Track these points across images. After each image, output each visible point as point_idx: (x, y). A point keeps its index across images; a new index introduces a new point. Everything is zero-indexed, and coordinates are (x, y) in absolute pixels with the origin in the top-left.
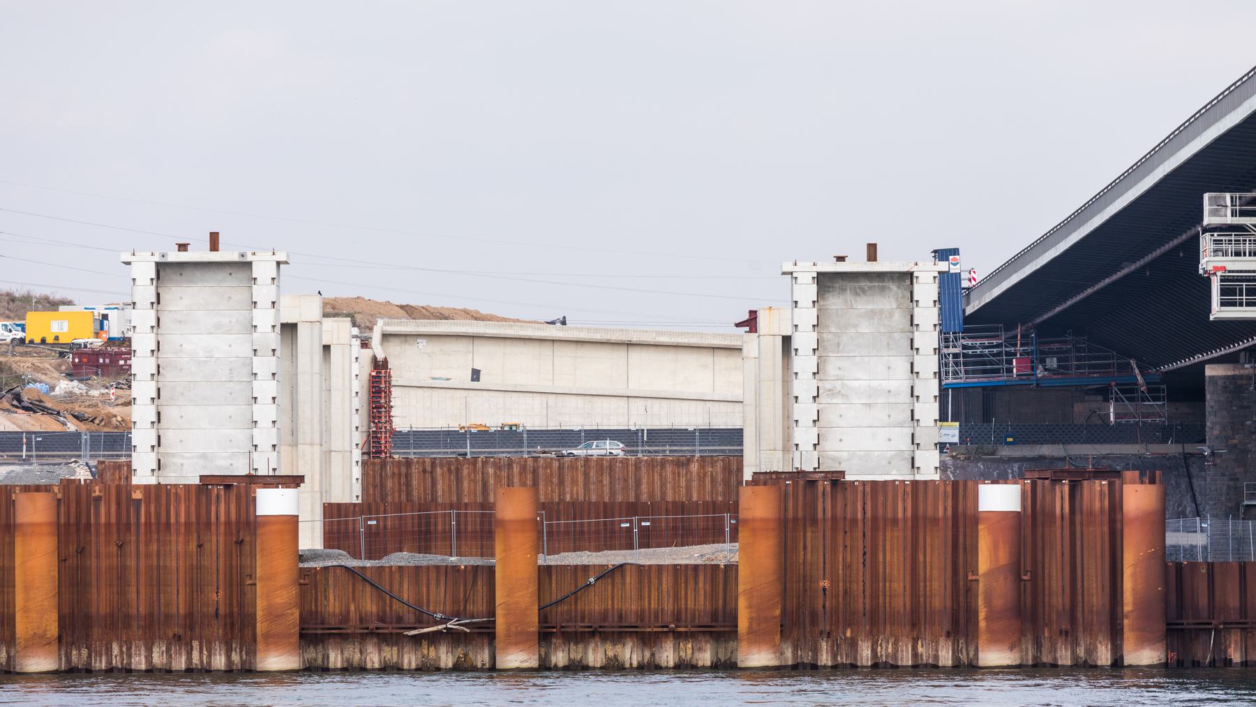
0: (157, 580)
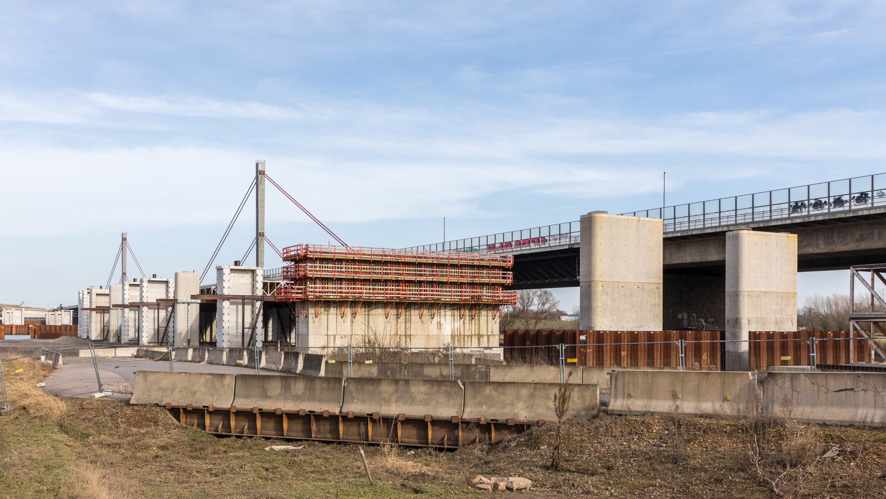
0: (22, 331)
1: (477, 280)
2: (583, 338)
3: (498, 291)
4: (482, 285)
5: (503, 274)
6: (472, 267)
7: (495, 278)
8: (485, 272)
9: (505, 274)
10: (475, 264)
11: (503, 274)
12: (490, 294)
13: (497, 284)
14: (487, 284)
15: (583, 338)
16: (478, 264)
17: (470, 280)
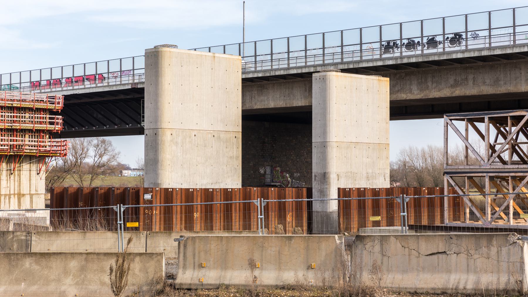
1: (17, 126)
2: (148, 197)
3: (44, 140)
4: (24, 131)
5: (50, 118)
6: (11, 109)
7: (41, 123)
8: (27, 115)
9: (53, 118)
10: (15, 105)
11: (50, 118)
12: (33, 143)
13: (43, 131)
14: (30, 131)
15: (148, 197)
16: (19, 105)
17: (8, 126)
